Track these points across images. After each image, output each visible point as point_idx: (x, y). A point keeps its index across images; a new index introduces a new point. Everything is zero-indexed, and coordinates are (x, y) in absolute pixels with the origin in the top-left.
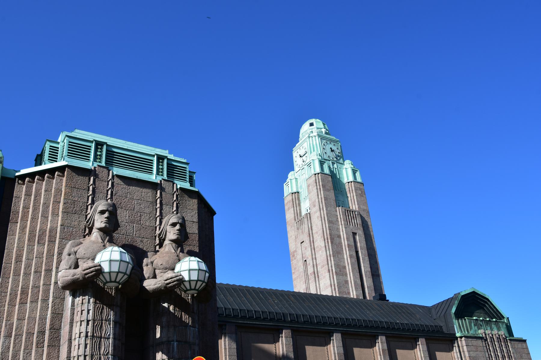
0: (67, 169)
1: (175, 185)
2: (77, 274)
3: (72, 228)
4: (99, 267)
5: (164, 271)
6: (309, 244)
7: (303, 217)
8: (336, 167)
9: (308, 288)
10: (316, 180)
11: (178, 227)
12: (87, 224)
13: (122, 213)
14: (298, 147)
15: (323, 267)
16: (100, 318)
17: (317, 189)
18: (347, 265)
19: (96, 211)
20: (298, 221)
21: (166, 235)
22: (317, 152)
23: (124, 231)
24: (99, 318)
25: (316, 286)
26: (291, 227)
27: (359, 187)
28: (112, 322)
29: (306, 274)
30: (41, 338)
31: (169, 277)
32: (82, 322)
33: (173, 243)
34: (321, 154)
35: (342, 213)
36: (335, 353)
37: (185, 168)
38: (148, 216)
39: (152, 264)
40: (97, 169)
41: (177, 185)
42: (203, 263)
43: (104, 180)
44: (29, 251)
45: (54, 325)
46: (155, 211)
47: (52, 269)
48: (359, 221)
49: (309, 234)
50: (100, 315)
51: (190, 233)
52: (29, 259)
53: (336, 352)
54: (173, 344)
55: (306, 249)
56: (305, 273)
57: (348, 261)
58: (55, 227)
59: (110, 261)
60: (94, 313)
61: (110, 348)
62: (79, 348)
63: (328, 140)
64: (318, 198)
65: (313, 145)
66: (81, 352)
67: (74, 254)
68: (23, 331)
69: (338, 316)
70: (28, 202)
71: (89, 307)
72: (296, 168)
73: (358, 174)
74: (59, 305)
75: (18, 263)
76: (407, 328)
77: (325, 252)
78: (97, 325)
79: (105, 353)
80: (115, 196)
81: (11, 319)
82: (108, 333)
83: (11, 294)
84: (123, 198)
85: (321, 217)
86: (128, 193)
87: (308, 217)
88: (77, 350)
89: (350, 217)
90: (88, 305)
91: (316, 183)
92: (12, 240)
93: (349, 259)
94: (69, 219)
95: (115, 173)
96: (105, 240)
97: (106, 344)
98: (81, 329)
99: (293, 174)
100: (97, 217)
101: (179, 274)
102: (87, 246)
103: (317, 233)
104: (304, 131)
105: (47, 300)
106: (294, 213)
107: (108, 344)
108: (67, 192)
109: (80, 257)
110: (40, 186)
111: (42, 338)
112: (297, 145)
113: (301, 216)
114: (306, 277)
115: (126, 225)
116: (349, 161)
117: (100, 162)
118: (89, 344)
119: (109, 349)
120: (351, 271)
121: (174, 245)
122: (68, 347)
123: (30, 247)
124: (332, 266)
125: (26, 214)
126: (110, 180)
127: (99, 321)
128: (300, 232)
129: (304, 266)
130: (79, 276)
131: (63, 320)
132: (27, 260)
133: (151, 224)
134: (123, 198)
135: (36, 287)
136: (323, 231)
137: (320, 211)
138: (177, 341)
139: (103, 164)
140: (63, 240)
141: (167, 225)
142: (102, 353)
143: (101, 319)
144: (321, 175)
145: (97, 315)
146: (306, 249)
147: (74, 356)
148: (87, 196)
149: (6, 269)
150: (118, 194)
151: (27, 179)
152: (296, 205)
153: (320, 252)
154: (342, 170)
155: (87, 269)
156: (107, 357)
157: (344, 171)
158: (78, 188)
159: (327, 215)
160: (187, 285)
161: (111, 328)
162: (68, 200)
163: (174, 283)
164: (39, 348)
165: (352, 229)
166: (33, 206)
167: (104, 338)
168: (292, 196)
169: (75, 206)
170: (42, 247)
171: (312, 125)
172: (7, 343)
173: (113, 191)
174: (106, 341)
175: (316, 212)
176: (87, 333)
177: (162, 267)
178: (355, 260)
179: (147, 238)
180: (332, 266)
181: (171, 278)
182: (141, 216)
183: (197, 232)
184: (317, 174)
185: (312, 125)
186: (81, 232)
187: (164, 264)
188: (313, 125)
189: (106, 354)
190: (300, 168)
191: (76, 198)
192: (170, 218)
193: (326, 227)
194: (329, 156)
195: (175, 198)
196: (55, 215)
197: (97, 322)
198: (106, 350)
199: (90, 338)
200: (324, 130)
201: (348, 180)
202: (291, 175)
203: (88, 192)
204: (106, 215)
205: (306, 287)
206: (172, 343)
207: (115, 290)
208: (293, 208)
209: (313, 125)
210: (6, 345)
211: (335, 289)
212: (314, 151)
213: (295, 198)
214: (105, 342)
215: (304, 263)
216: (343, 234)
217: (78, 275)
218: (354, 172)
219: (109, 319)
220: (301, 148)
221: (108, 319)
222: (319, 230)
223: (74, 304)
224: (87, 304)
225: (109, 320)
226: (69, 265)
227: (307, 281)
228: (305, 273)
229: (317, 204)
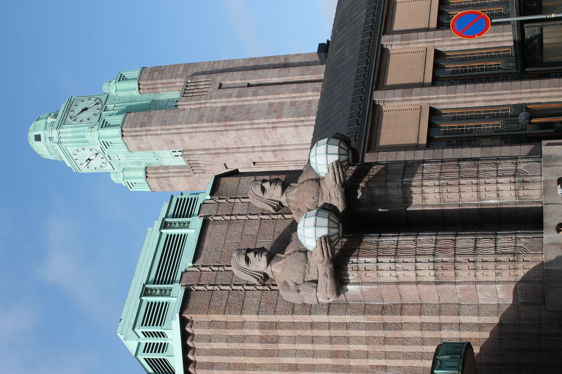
0: (184, 315)
2: (325, 271)
5: (321, 195)
6: (230, 156)
7: (188, 161)
8: (114, 105)
9: (296, 163)
10: (132, 136)
11: (267, 185)
12: (260, 280)
14: (74, 163)
15: (267, 136)
17: (146, 135)
18: (267, 101)
19: (245, 269)
20: (193, 170)
21: (275, 201)
22: (86, 131)
24: (375, 252)
25: (293, 150)
26: (199, 183)
27: (147, 74)
28: (379, 240)
29: (274, 164)
31: (333, 177)
33: (285, 192)
34: (90, 125)
35: (188, 101)
36: (402, 101)
37: (178, 199)
40: (184, 284)
42: (318, 142)
47: (310, 322)
48: (202, 78)
49: (215, 154)
50: (372, 251)
52: (296, 354)
53: (401, 98)
54: (406, 181)
55: (237, 161)
56: (273, 166)
57: (262, 100)
59: (315, 226)
61: (409, 239)
63: (66, 114)
64: (161, 134)
65: (74, 137)
67: (298, 286)
68: (381, 351)
69: (350, 97)
72: (108, 168)
73: (127, 74)
76: (372, 10)
77: (246, 131)
78: (382, 253)
81: (366, 368)
83: (336, 371)
85: (192, 133)
87: (188, 153)
88: (410, 271)
89: (195, 91)
91: (136, 136)
93: (258, 98)
95: (191, 264)
96: (281, 257)
99: (115, 175)
100: (252, 268)
101: (331, 165)
102: (290, 272)
103: (214, 142)
104: (47, 151)
106: (178, 177)
107: (404, 241)
109: (303, 278)
112: (69, 165)
113: (184, 167)
114: (278, 165)
116: (104, 85)
118: (404, 259)
120: (277, 96)
121: (288, 190)
122: (405, 285)
124: (268, 123)
126: (200, 269)
128: (209, 169)
129: (262, 167)
130: (327, 269)
131: (372, 303)
133: (256, 223)
134: (224, 254)
135: (331, 340)
136: (213, 131)
137: (181, 133)
138: (403, 178)
140: (277, 310)
144: (126, 128)
146: (237, 161)
150: (217, 260)
152: (166, 173)
153: (244, 139)
154: (119, 97)
157: (121, 94)
159: (190, 123)
161: (387, 239)
164: (402, 328)
165: (214, 90)
166: (229, 356)
167: (397, 245)
168: (150, 178)
171: (38, 138)
175: (183, 140)
177: (316, 198)
178: (260, 90)
180: (268, 123)
182: (247, 235)
184: (123, 133)
185: (38, 138)
186: (267, 294)
187: (312, 195)
188: (36, 140)
189: (415, 243)
190: (108, 163)
191: (223, 302)
192: (254, 194)
193: (207, 127)
194: (94, 115)
195: (224, 201)
198: (410, 243)
199: (397, 258)
200: (50, 120)
201: (136, 90)
202: (117, 178)
205: (293, 166)
206: (404, 183)
208: (171, 179)
209: (36, 140)
211: (302, 121)
212: (84, 137)
213: (155, 173)
214: (402, 244)
215: (257, 166)
216: (220, 103)
217: (326, 269)
218: (122, 78)
219: (376, 242)
220: (75, 157)
222: (211, 137)
223: (356, 283)
227: (284, 164)
228: (273, 166)
229: (170, 137)
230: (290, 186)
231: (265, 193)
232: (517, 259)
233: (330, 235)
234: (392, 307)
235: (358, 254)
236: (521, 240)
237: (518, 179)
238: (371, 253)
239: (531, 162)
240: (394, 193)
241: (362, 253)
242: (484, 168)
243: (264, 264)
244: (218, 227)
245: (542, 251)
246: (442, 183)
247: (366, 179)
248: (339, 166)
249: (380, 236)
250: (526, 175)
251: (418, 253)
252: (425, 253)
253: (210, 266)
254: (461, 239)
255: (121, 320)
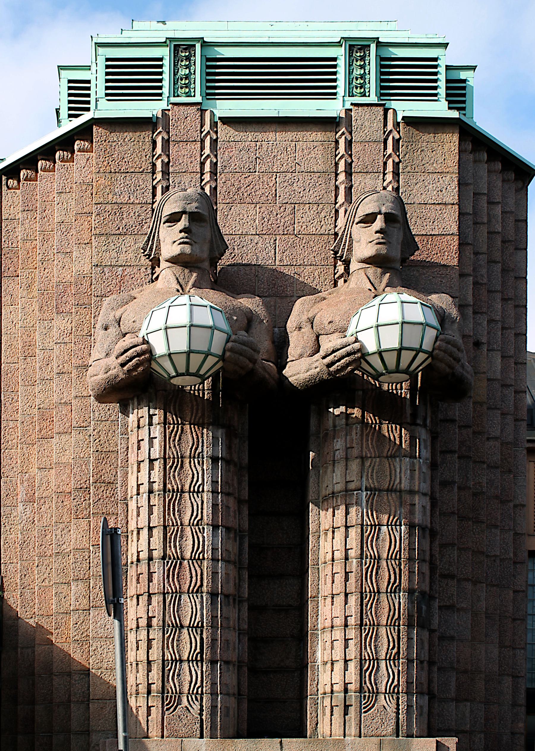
1: (390, 113)
2: (113, 367)
3: (121, 268)
4: (144, 346)
13: (244, 212)
16: (177, 453)
23: (249, 255)
30: (82, 500)
32: (142, 464)
33: (368, 266)
38: (314, 209)
39: (312, 323)
41: (398, 112)
43: (191, 139)
44: (45, 331)
45: (102, 473)
46: (333, 195)
51: (434, 235)
58: (85, 272)
60: (163, 443)
62: (138, 515)
66: (143, 522)
67: (116, 325)
70: (32, 227)
71: (151, 432)
74: (109, 434)
75: (29, 359)
79: (194, 520)
80: (223, 175)
82: (197, 481)
84: (243, 176)
86: (256, 159)
90: (149, 429)
92: (12, 313)
94: (113, 247)
97: (195, 504)
98: (139, 478)
105: (86, 427)
108: (102, 187)
110: (50, 185)
111: (84, 501)
115: (256, 242)
117: (188, 95)
119: (202, 513)
123: (46, 322)
125: (31, 254)
127: (176, 460)
130: (116, 370)
132: (43, 351)
133: (324, 226)
134: (243, 176)
139: (373, 99)
141: (353, 223)
142: (188, 521)
143: (181, 454)
145: (170, 447)
147: (133, 529)
148: (151, 187)
149: (9, 375)
151: (23, 173)
155: (123, 354)
156: (199, 529)
158: (128, 172)
160: (376, 362)
162: (104, 206)
163: (342, 361)
164: (80, 518)
169: (124, 216)
170: (66, 319)
172: (28, 513)
173: (217, 162)
174: (194, 498)
176: (151, 483)
179: (311, 265)
181: (334, 352)
183: (454, 229)
186: (143, 275)
187: (337, 319)
189: (195, 522)
192: (358, 203)
196: (84, 246)
197: (171, 462)
203: (153, 176)
204: (184, 222)
207: (210, 391)
210: (28, 516)
221: (197, 453)
224: (147, 427)
225: (200, 455)
226: (104, 351)
230: (383, 274)
231: (362, 225)
232: (154, 696)
233: (159, 360)
234: (111, 497)
235: (170, 424)
236: (196, 702)
237: (353, 697)
238: (172, 446)
239: (202, 720)
240: (336, 476)
241: (172, 431)
242: (385, 637)
243: (167, 254)
244: (319, 153)
245: (168, 737)
246: (352, 561)
247: (369, 418)
248: (352, 357)
249: (214, 460)
250: (363, 711)
251: (170, 529)
252: (170, 542)
253: (216, 156)
254: (202, 602)
255: (164, 23)
